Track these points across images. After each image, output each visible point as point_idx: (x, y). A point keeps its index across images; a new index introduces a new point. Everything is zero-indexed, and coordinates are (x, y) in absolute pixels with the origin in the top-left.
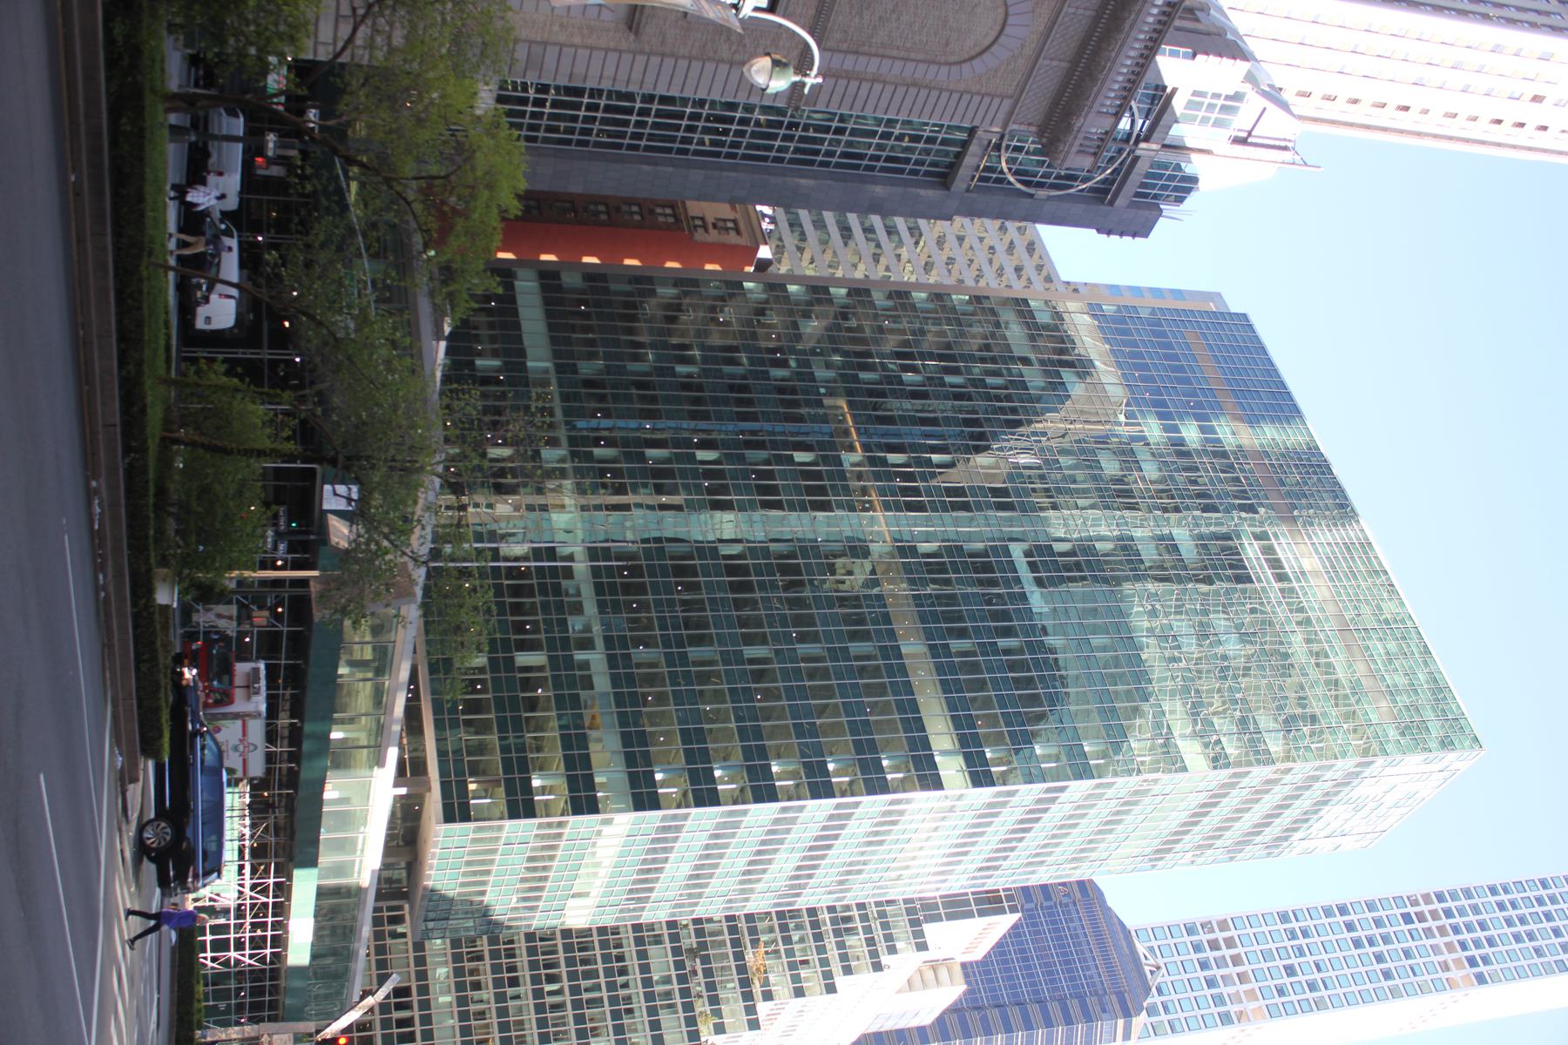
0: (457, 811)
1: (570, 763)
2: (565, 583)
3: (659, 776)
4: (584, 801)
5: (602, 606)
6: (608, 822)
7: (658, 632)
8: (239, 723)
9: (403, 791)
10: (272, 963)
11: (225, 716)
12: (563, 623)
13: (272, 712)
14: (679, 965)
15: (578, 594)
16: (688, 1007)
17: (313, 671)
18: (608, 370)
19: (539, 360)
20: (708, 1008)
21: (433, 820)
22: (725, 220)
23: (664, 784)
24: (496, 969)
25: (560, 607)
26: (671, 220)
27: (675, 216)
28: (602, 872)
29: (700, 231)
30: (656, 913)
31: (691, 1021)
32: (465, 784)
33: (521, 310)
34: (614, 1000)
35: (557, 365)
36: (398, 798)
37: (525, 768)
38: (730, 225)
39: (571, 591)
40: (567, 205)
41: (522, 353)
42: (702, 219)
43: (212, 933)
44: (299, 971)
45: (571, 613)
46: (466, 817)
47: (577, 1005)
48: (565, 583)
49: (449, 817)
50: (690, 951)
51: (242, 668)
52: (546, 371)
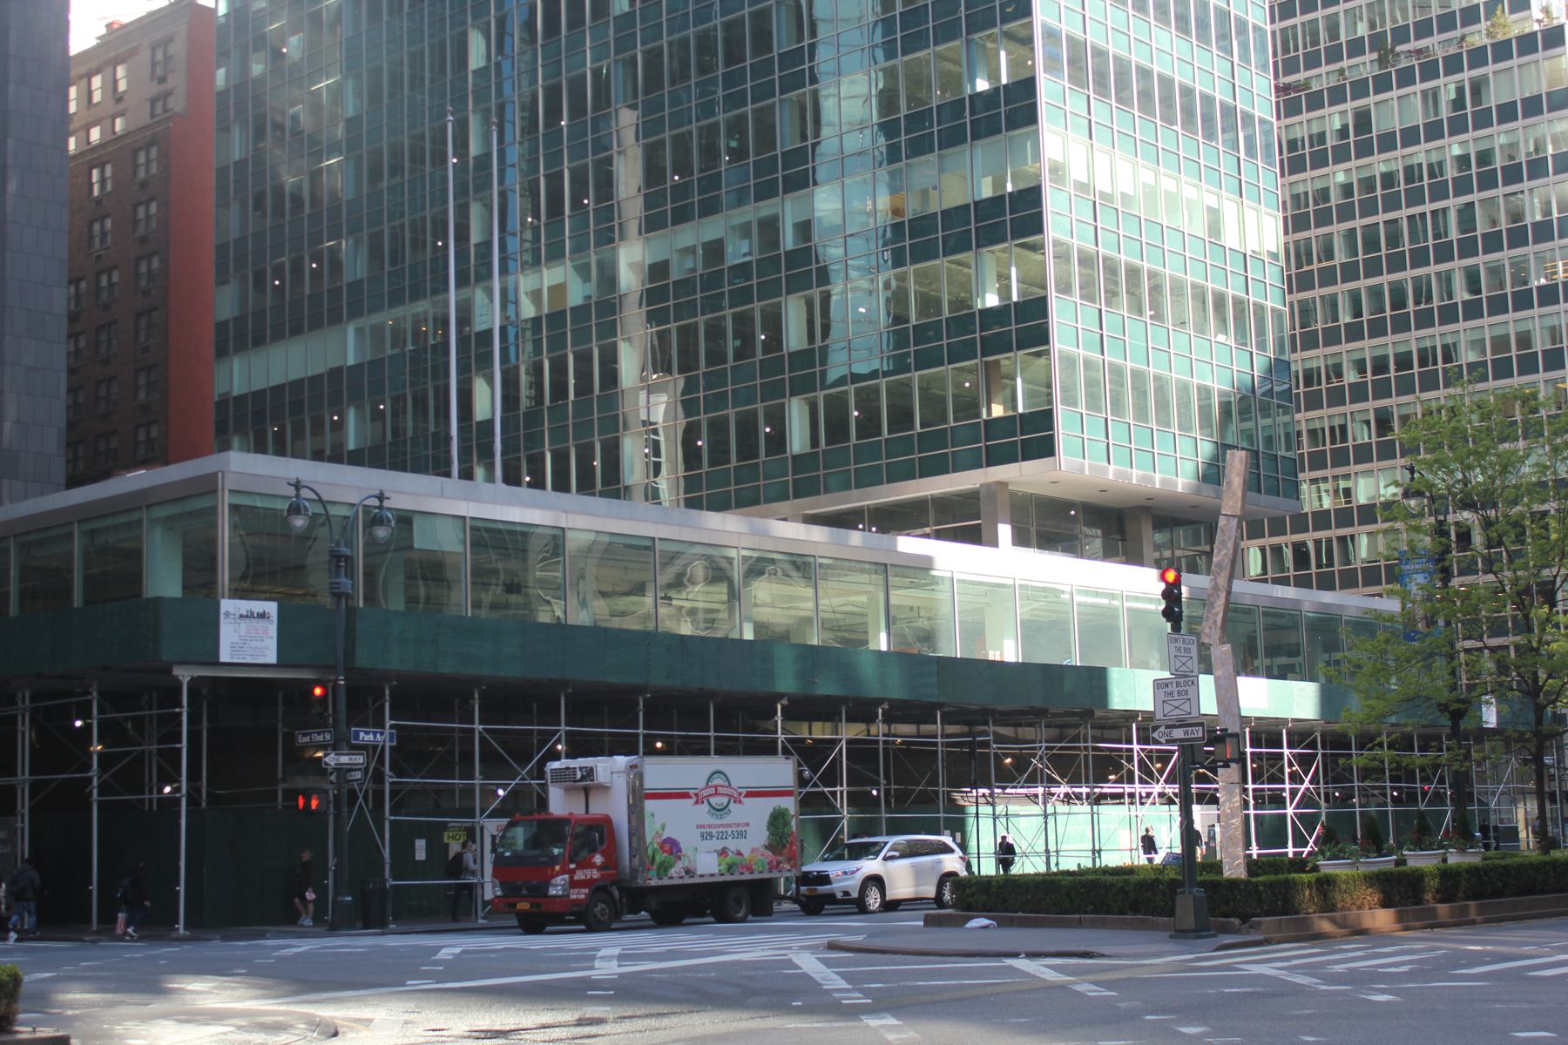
0: (1033, 436)
1: (959, 244)
3: (982, 85)
4: (1019, 215)
5: (710, 208)
6: (1058, 171)
7: (749, 107)
8: (649, 805)
9: (1005, 531)
10: (1313, 745)
11: (637, 830)
12: (742, 270)
13: (625, 746)
14: (1406, 78)
15: (691, 250)
16: (1478, 58)
17: (658, 679)
18: (354, 230)
19: (346, 346)
20: (1483, 25)
21: (1054, 476)
22: (154, 63)
23: (994, 75)
24: (1406, 387)
25: (712, 280)
26: (154, 152)
27: (148, 146)
28: (1168, 184)
29: (171, 103)
30: (1257, 93)
31: (1502, 50)
32: (992, 424)
33: (293, 376)
34: (1463, 186)
36: (1021, 539)
37: (965, 318)
38: (159, 56)
39: (689, 264)
41: (336, 373)
42: (153, 102)
44: (1328, 700)
46: (1044, 419)
47: (1468, 248)
48: (675, 275)
49: (1045, 448)
50: (1382, 62)
51: (559, 803)
52: (359, 332)
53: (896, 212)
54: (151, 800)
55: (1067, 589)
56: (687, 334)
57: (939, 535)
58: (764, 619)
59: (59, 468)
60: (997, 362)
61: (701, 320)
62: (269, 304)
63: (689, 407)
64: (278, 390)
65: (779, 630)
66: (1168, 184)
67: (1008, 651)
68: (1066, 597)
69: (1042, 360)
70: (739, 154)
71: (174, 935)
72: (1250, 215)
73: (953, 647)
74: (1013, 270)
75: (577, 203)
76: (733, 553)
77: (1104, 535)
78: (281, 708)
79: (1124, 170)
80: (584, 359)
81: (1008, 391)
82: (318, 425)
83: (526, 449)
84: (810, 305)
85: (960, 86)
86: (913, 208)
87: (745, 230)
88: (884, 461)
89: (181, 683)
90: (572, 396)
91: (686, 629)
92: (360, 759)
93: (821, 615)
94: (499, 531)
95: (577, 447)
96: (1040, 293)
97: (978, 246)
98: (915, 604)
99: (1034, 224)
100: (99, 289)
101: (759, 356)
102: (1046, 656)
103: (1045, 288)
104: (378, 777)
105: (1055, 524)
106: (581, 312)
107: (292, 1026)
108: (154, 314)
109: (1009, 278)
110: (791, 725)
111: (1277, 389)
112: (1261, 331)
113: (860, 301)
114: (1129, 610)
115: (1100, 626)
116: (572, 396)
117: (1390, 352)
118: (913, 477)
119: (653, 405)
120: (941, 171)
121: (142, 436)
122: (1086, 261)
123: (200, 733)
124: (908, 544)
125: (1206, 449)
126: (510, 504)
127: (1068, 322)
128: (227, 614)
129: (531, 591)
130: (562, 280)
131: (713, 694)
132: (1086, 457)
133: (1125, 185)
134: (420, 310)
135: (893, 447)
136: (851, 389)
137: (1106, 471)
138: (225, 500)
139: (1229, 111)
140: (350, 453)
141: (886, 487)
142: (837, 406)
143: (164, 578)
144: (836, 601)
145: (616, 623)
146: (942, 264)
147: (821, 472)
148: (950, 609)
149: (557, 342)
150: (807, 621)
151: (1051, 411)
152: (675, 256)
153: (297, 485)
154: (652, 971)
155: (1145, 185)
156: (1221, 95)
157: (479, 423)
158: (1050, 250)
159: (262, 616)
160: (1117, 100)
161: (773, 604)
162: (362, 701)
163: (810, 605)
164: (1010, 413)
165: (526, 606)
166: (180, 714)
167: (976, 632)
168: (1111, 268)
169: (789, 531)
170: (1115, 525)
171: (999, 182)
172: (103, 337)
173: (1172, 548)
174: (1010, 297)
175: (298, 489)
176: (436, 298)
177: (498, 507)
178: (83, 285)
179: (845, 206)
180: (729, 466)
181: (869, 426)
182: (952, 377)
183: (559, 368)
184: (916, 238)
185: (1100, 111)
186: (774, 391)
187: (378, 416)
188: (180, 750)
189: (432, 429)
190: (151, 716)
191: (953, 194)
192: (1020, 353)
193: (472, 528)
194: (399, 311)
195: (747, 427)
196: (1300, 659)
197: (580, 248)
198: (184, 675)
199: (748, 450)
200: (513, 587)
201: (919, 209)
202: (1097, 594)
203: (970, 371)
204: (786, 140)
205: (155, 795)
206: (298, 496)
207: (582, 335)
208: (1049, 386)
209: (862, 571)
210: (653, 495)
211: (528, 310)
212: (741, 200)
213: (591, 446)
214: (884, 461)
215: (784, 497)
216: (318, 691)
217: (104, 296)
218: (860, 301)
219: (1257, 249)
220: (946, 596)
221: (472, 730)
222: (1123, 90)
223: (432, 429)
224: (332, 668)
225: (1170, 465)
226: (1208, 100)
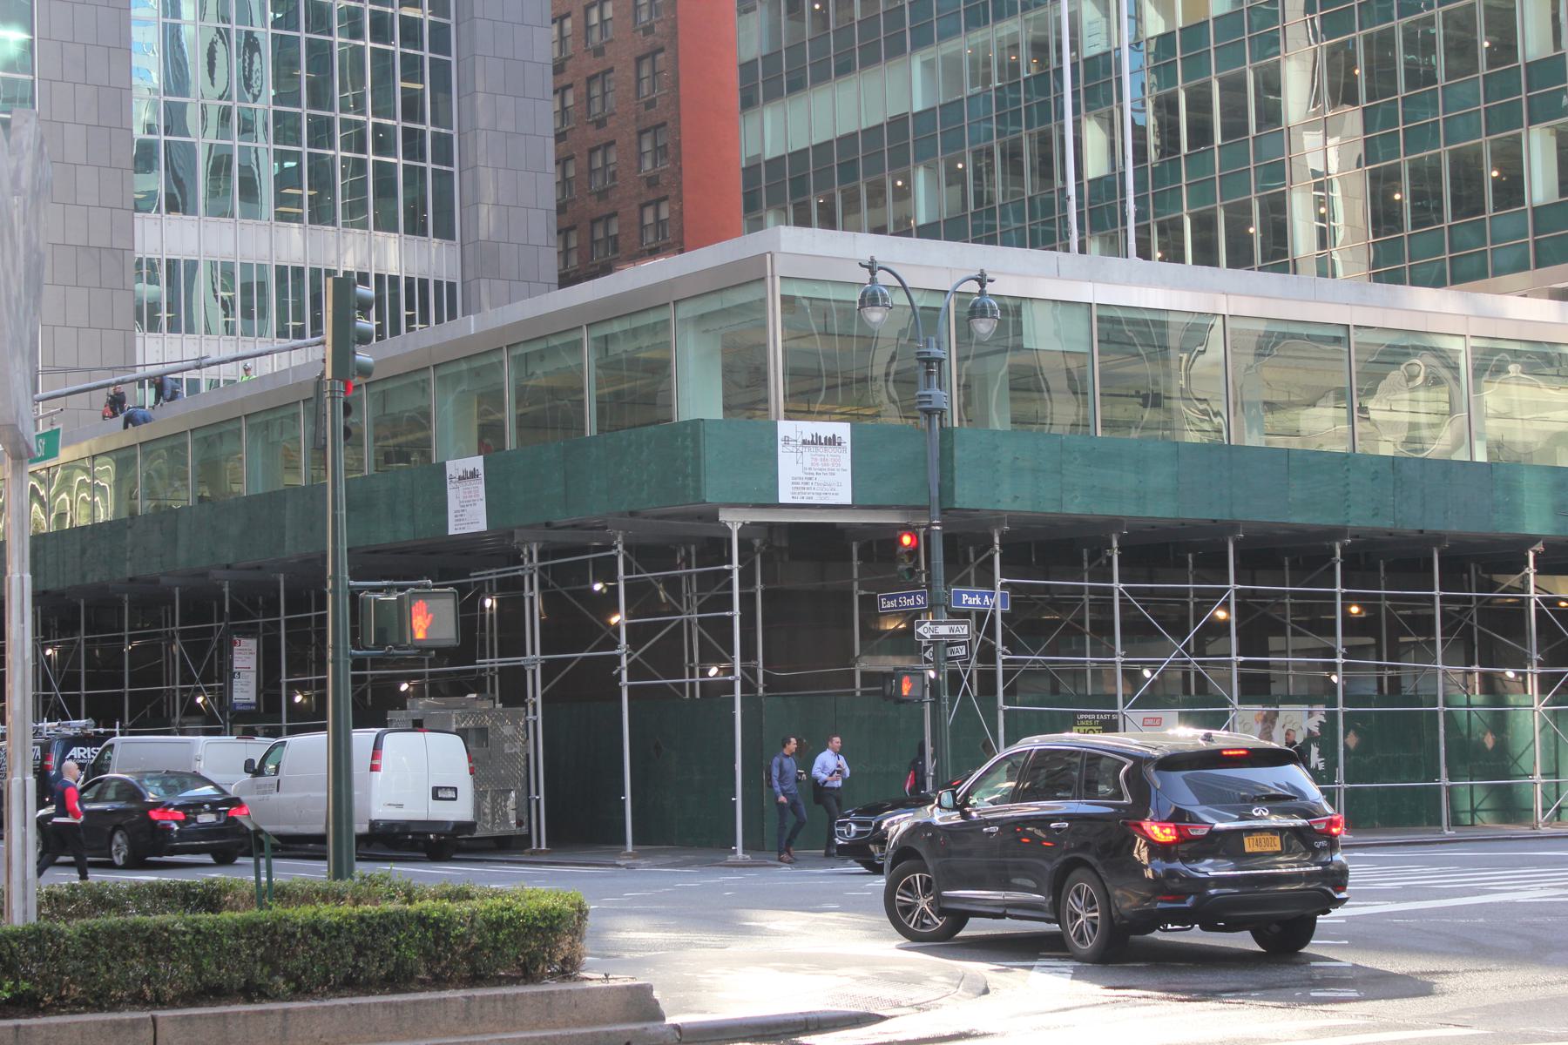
17: (1361, 516)
33: (843, 130)
35: (917, 46)
40: (645, 71)
41: (899, 123)
43: (1335, 664)
52: (928, 65)
54: (692, 685)
59: (550, 263)
62: (808, 35)
64: (823, 149)
65: (1519, 449)
71: (731, 858)
76: (1457, 344)
78: (856, 563)
80: (1234, 87)
82: (877, 193)
89: (730, 531)
90: (1218, 140)
92: (963, 630)
100: (588, 28)
101: (1483, 69)
104: (987, 654)
107: (927, 979)
108: (660, 57)
110: (1546, 580)
116: (1218, 140)
119: (1325, 153)
121: (649, 218)
123: (754, 595)
126: (1150, 284)
128: (787, 440)
131: (1437, 538)
134: (1005, 33)
138: (777, 290)
140: (918, 228)
143: (698, 396)
149: (1196, 65)
153: (872, 267)
154: (1390, 914)
159: (832, 441)
162: (964, 548)
165: (1167, 425)
166: (730, 572)
172: (596, 91)
175: (873, 273)
176: (1032, 15)
177: (1135, 290)
178: (568, 24)
183: (1199, 103)
186: (1504, 118)
187: (955, 178)
188: (731, 618)
190: (689, 576)
193: (1100, 319)
194: (978, 36)
198: (734, 520)
199: (1468, 203)
200: (1154, 400)
205: (697, 679)
206: (873, 281)
207: (1231, 54)
210: (1325, 269)
213: (1247, 206)
215: (1522, 266)
216: (907, 540)
217: (595, 35)
221: (1110, 591)
223: (1028, 192)
224: (924, 509)
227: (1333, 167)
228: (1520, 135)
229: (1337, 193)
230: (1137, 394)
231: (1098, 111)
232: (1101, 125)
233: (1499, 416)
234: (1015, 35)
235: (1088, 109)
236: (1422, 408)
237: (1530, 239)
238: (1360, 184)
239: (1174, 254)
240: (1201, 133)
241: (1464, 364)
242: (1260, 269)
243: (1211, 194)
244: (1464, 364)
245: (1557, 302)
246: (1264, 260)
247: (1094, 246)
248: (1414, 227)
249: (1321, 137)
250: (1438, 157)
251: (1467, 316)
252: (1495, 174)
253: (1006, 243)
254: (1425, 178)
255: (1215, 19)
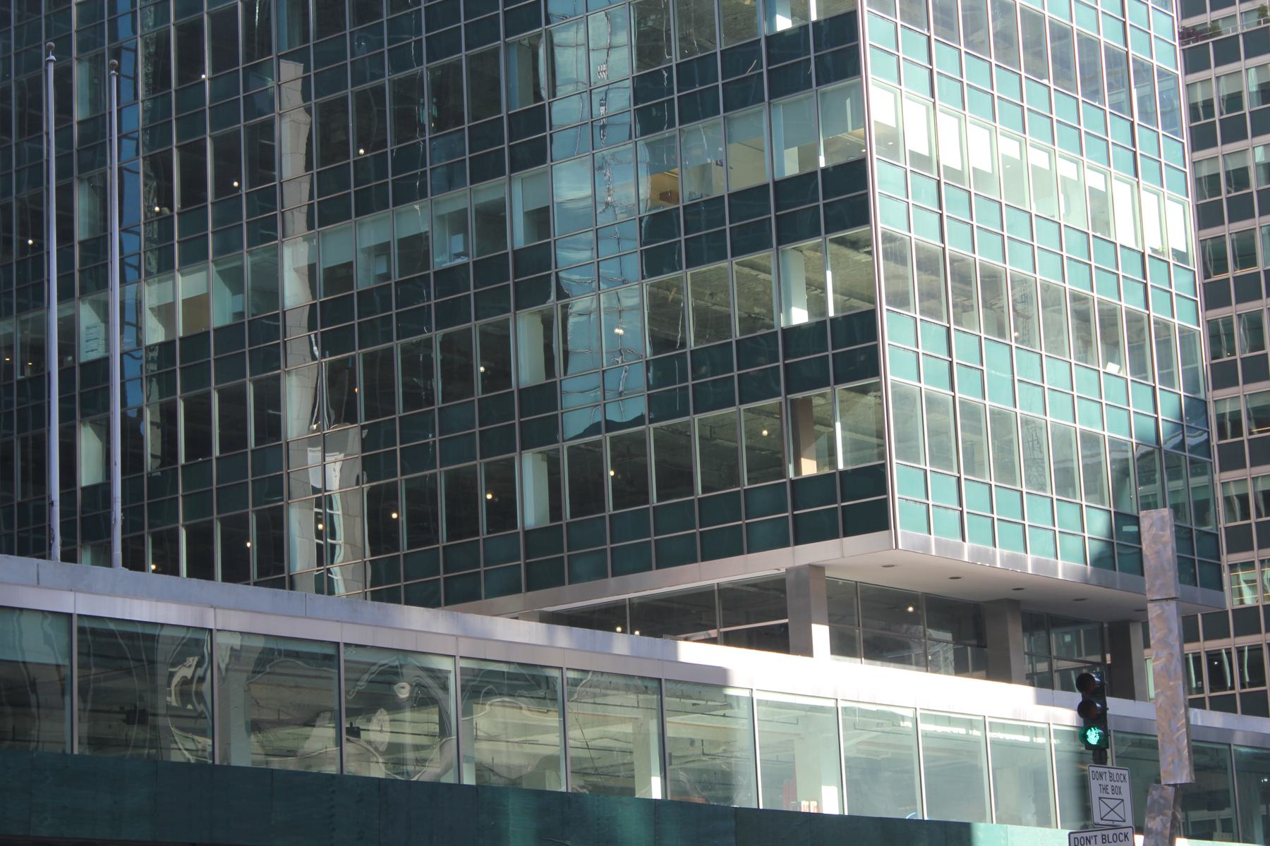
0: (859, 501)
1: (750, 240)
2: (363, 281)
4: (836, 199)
5: (406, 194)
6: (892, 141)
9: (821, 634)
12: (450, 278)
21: (889, 556)
25: (410, 290)
28: (1038, 158)
32: (802, 485)
36: (842, 646)
45: (425, 262)
48: (363, 281)
49: (875, 518)
53: (667, 196)
55: (910, 713)
56: (379, 365)
57: (729, 640)
58: (486, 759)
60: (808, 401)
61: (397, 344)
63: (372, 467)
66: (1038, 158)
67: (829, 801)
68: (908, 724)
69: (870, 399)
70: (447, 118)
72: (1149, 201)
73: (754, 795)
74: (829, 274)
75: (223, 186)
76: (446, 665)
77: (957, 639)
79: (978, 137)
80: (233, 400)
81: (823, 441)
83: (150, 526)
84: (547, 324)
85: (751, 25)
86: (689, 190)
87: (457, 222)
88: (652, 538)
90: (216, 451)
91: (378, 770)
93: (571, 753)
94: (111, 634)
95: (223, 521)
96: (866, 307)
97: (779, 243)
98: (698, 735)
99: (860, 212)
101: (478, 393)
102: (884, 807)
103: (872, 300)
105: (885, 624)
106: (229, 334)
109: (823, 288)
111: (1190, 441)
112: (1166, 362)
113: (605, 326)
114: (994, 742)
115: (956, 763)
116: (216, 451)
117: (1242, 407)
118: (694, 561)
119: (327, 471)
120: (728, 139)
122: (929, 263)
124: (694, 652)
125: (1097, 523)
126: (135, 595)
127: (904, 342)
129: (161, 721)
130: (189, 294)
132: (936, 530)
133: (980, 159)
135: (665, 518)
136: (606, 438)
137: (959, 550)
139: (1118, 60)
141: (655, 574)
142: (586, 459)
144: (590, 733)
145: (276, 763)
146: (729, 266)
147: (565, 554)
148: (749, 743)
149: (196, 376)
150: (550, 762)
151: (883, 466)
152: (360, 256)
155: (1007, 159)
156: (1108, 37)
157: (83, 489)
158: (879, 247)
160: (967, 45)
161: (508, 739)
163: (555, 738)
164: (827, 471)
165: (154, 743)
167: (783, 775)
168: (962, 276)
169: (512, 632)
170: (976, 626)
171: (808, 155)
173: (1049, 658)
174: (825, 312)
177: (119, 600)
179: (592, 188)
180: (435, 540)
181: (632, 489)
182: (747, 422)
183: (198, 414)
184: (678, 235)
185: (945, 58)
186: (499, 443)
189: (18, 497)
191: (745, 174)
192: (840, 387)
193: (81, 630)
195: (462, 492)
196: (1226, 813)
197: (227, 246)
199: (462, 523)
201: (698, 194)
202: (950, 721)
203: (769, 413)
204: (512, 101)
207: (230, 368)
208: (880, 435)
209: (627, 688)
210: (324, 586)
211: (155, 333)
212: (451, 181)
213: (244, 520)
214: (652, 538)
215: (515, 590)
218: (605, 326)
219: (1158, 246)
220: (743, 724)
222: (975, 30)
223: (18, 497)
225: (1051, 544)
226: (1089, 45)
227: (334, 483)
228: (513, 458)
229: (338, 512)
230: (122, 711)
231: (93, 417)
232: (99, 436)
233: (490, 739)
234: (10, 335)
235: (83, 416)
236: (408, 728)
237: (522, 562)
238: (360, 505)
239: (168, 566)
240: (199, 443)
241: (453, 684)
242: (256, 584)
243: (213, 509)
244: (453, 684)
245: (544, 625)
246: (259, 575)
247: (86, 556)
248: (409, 547)
249: (320, 454)
250: (434, 477)
251: (457, 637)
252: (489, 496)
253: (22, 553)
254: (421, 497)
255: (216, 330)
